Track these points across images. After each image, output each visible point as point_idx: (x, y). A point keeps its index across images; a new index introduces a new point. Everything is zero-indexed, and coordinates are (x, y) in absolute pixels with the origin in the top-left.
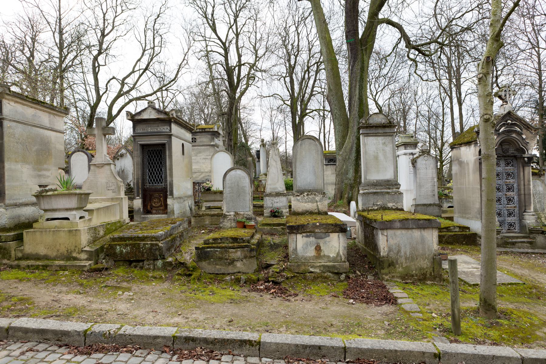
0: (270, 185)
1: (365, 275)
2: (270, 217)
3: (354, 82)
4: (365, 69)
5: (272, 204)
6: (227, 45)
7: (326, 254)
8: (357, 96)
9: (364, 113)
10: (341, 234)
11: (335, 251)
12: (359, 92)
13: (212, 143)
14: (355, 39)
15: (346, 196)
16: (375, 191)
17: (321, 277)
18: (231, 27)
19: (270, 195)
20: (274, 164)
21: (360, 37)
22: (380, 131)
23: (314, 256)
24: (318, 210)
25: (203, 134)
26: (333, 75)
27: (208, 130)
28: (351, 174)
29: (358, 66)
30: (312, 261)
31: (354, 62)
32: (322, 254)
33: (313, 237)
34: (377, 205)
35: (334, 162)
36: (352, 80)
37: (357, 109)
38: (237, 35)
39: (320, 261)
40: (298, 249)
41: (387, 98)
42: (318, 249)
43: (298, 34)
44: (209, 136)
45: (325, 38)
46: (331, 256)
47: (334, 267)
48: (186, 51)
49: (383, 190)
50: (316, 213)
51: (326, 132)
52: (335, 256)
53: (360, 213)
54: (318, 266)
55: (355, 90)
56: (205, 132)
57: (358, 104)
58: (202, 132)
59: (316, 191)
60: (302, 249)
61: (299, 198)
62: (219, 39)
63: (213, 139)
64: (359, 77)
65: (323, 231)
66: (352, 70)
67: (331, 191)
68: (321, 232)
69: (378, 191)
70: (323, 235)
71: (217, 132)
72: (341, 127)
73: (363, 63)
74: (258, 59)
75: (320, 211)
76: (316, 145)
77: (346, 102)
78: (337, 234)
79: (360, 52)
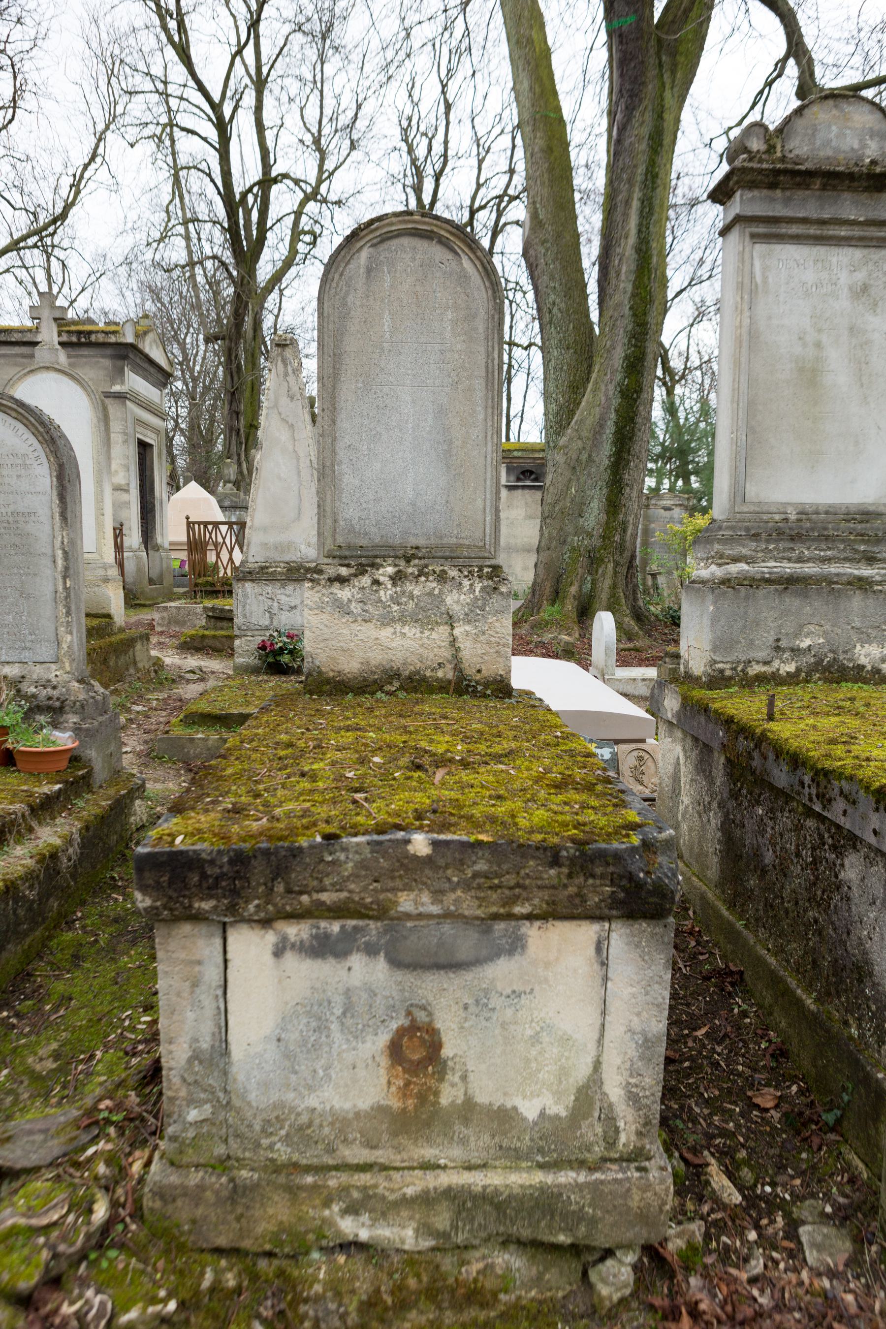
0: (265, 529)
1: (773, 1204)
2: (256, 671)
3: (624, 187)
4: (667, 141)
5: (272, 616)
6: (227, 111)
7: (485, 1093)
8: (632, 240)
9: (651, 301)
10: (620, 937)
11: (563, 1073)
12: (640, 225)
13: (117, 388)
14: (640, 19)
15: (573, 590)
16: (788, 568)
17: (432, 1293)
18: (239, 52)
19: (260, 574)
20: (284, 435)
21: (657, 15)
22: (850, 207)
23: (381, 1110)
24: (458, 669)
25: (85, 351)
26: (551, 170)
27: (101, 338)
28: (594, 515)
29: (641, 128)
30: (356, 1154)
31: (630, 110)
32: (449, 1095)
33: (371, 951)
34: (796, 651)
35: (536, 480)
36: (619, 178)
37: (630, 288)
38: (260, 84)
39: (428, 1153)
40: (237, 1051)
41: (686, 324)
42: (417, 1051)
43: (448, 107)
44: (107, 363)
45: (530, 41)
46: (530, 1110)
47: (546, 1203)
48: (101, 127)
49: (833, 569)
50: (443, 687)
51: (512, 414)
52: (559, 1109)
53: (698, 693)
54: (406, 1202)
55: (626, 215)
56: (90, 345)
57: (633, 267)
58: (79, 345)
59: (451, 556)
60: (272, 1052)
61: (344, 593)
62: (201, 88)
63: (121, 372)
64: (641, 169)
65: (469, 907)
66: (619, 141)
67: (522, 573)
68: (447, 915)
69: (810, 569)
70: (466, 943)
71: (132, 346)
72: (569, 355)
73: (660, 117)
74: (326, 175)
75: (470, 671)
76: (464, 278)
77: (590, 252)
78: (585, 933)
79: (652, 73)
